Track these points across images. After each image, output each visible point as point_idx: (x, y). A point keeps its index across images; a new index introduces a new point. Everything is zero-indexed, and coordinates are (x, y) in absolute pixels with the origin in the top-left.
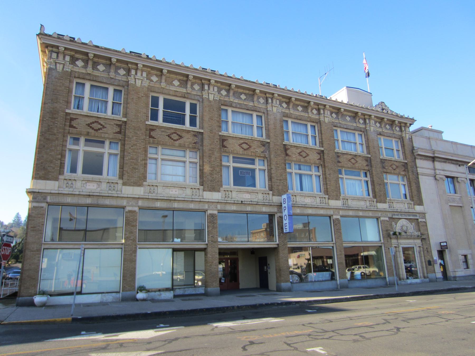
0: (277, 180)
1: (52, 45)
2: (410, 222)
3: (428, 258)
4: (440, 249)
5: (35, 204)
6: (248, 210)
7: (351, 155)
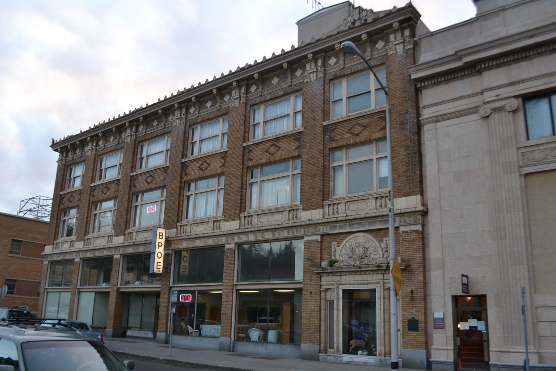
0: (170, 210)
1: (55, 146)
2: (376, 237)
3: (415, 313)
4: (459, 293)
5: (166, 252)
6: (266, 237)
7: (269, 141)
